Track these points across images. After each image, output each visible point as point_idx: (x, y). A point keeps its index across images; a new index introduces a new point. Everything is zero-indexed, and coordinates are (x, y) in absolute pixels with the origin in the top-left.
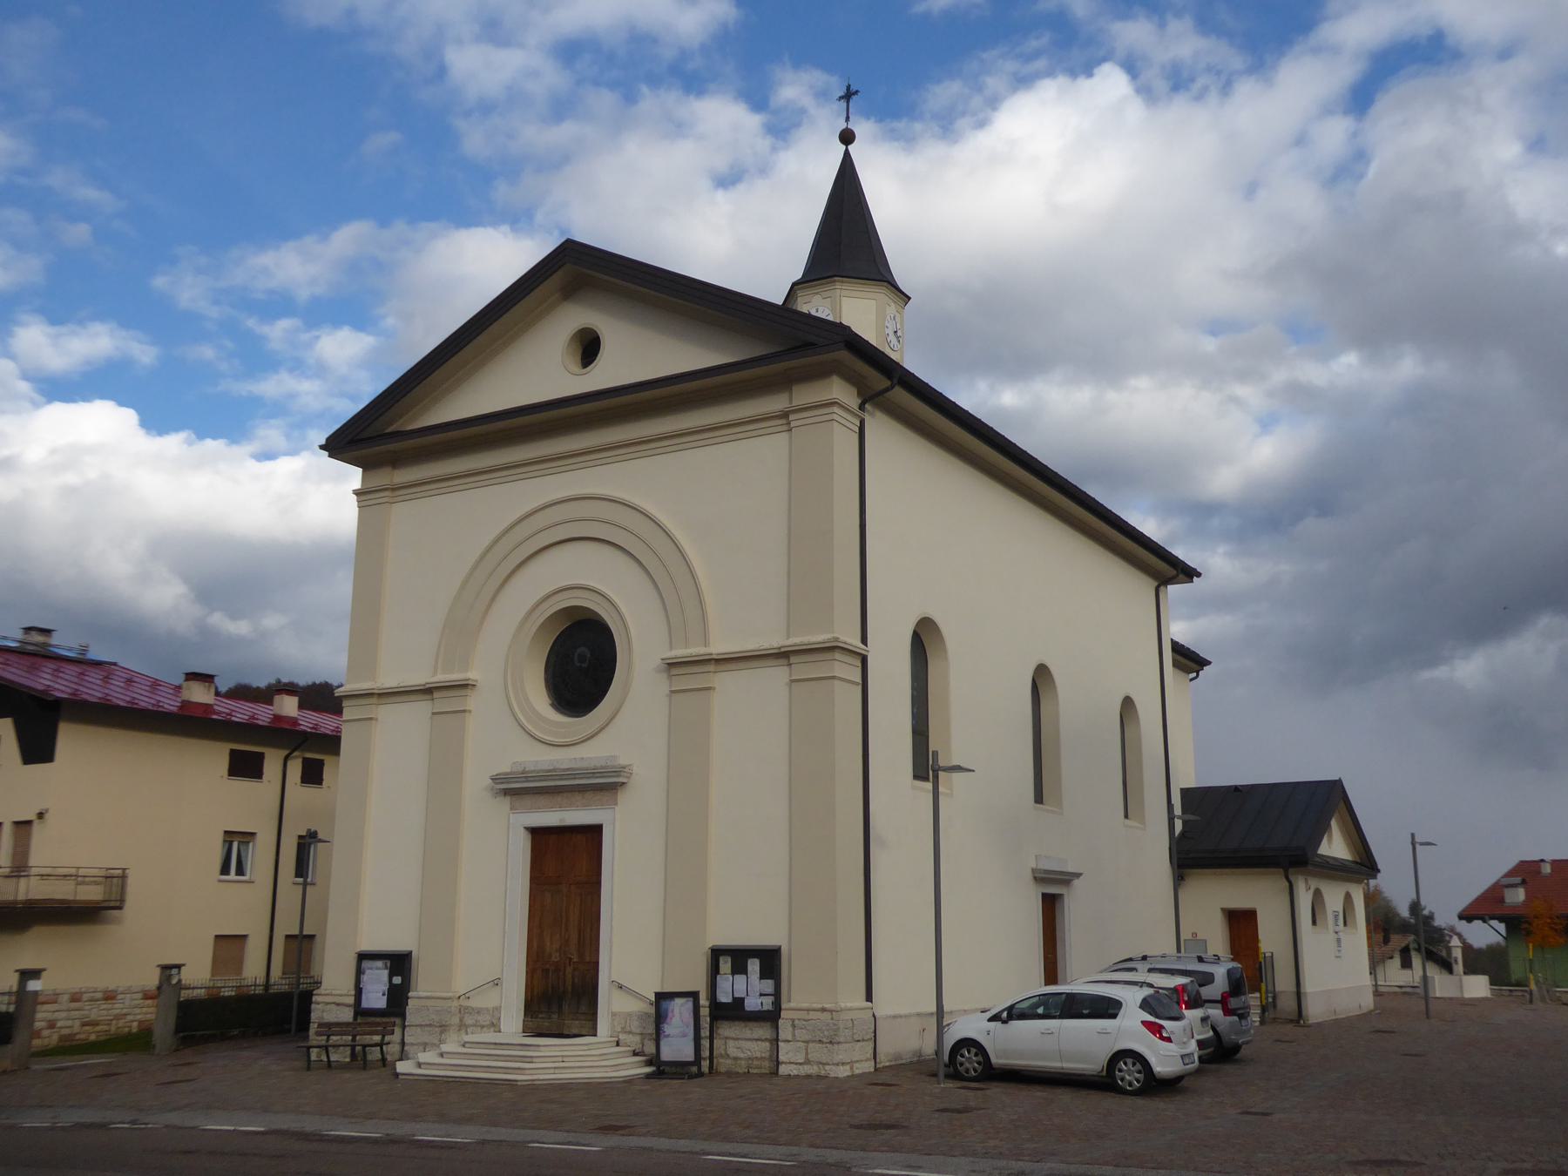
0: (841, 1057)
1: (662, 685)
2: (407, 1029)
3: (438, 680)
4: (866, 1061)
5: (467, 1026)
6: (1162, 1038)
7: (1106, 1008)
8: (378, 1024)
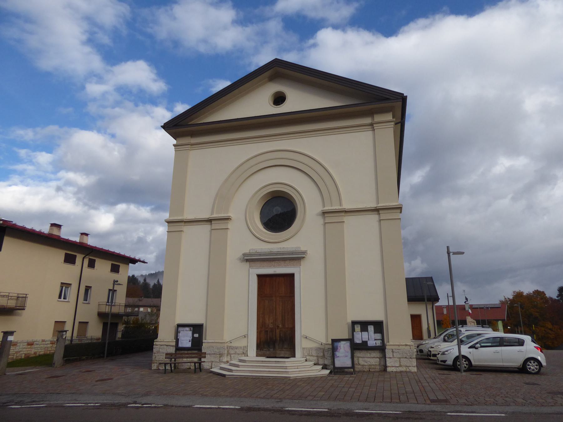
1: (320, 221)
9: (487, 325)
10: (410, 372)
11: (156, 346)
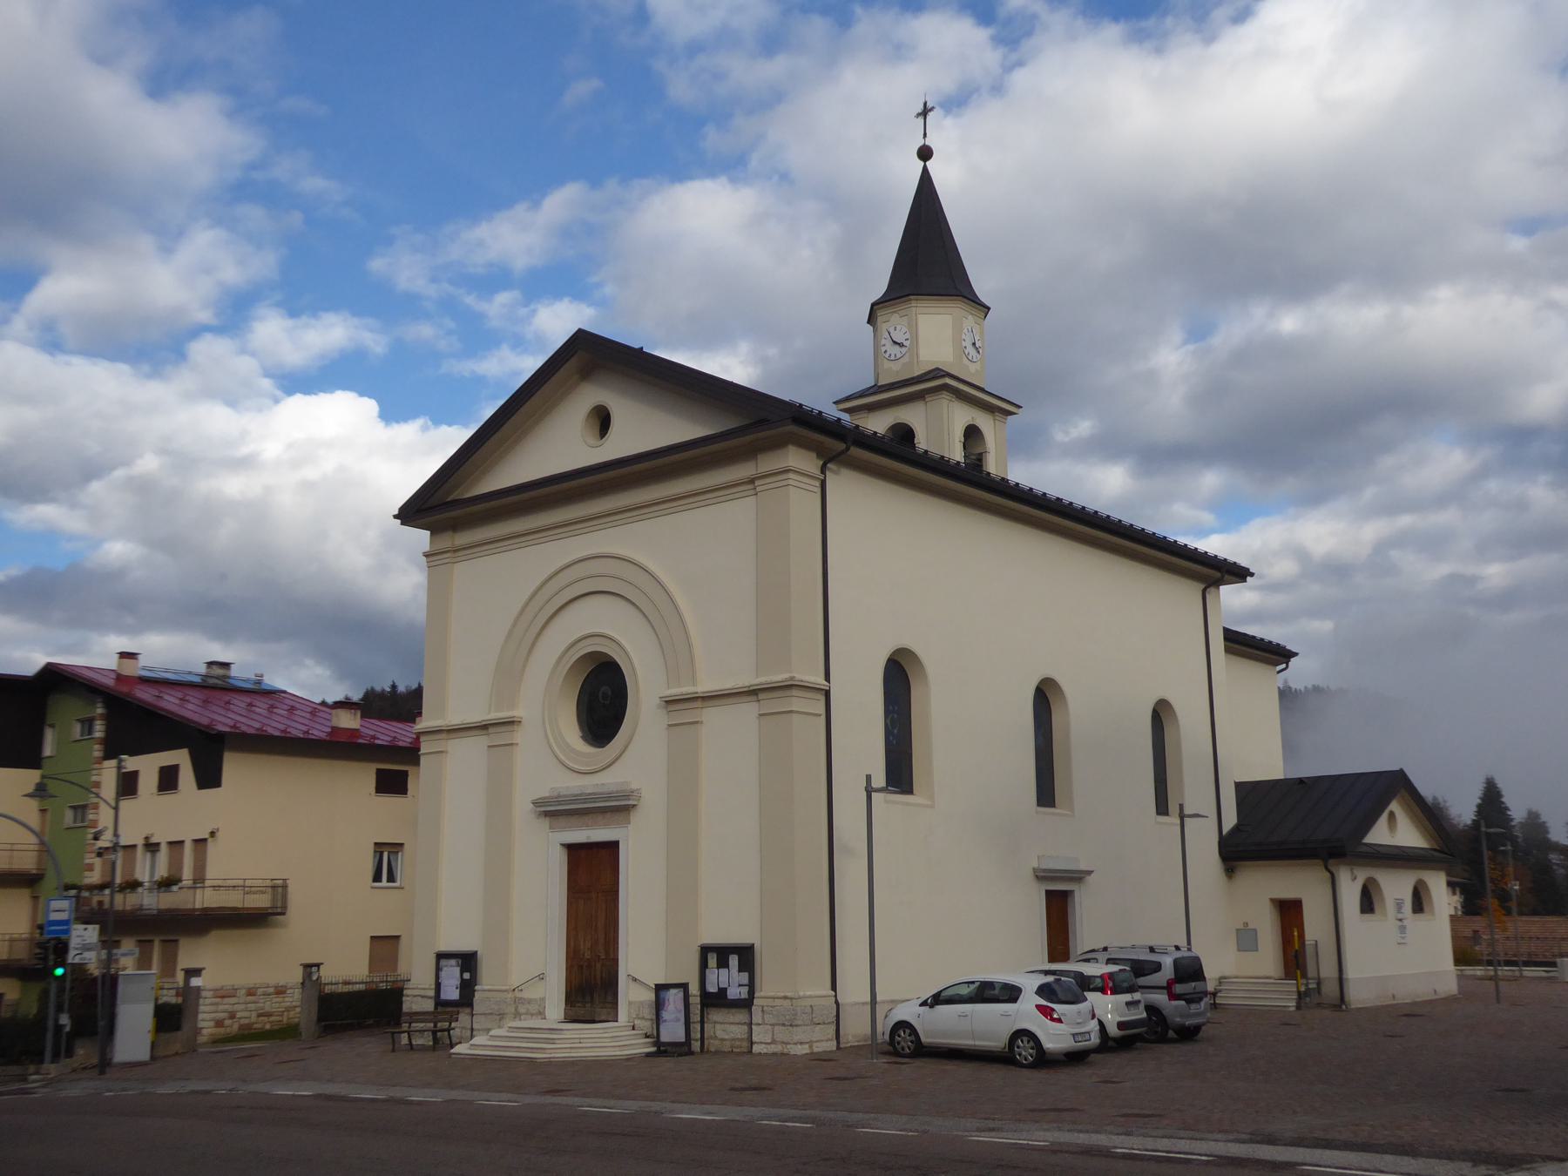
0: (798, 1037)
2: (474, 1017)
3: (494, 718)
4: (827, 1041)
5: (520, 1015)
6: (1053, 1020)
7: (1011, 994)
8: (447, 1013)
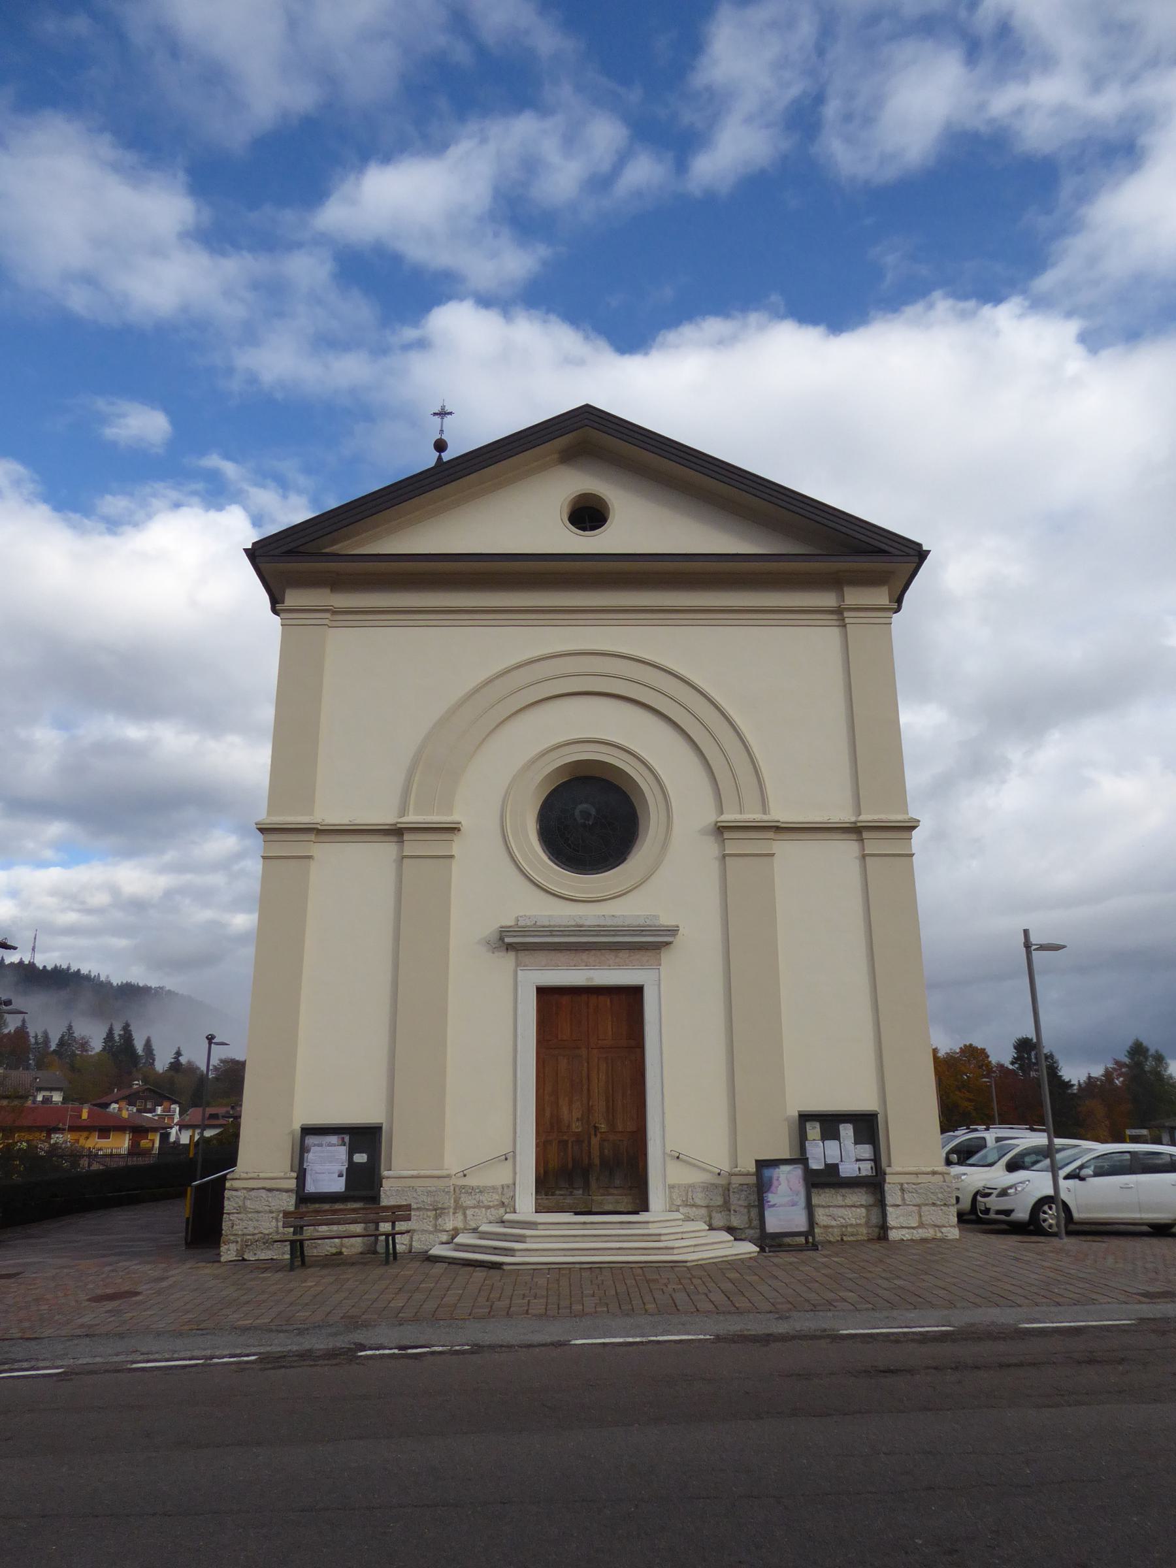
1: (711, 848)
9: (997, 1121)
10: (944, 1240)
11: (234, 1193)
